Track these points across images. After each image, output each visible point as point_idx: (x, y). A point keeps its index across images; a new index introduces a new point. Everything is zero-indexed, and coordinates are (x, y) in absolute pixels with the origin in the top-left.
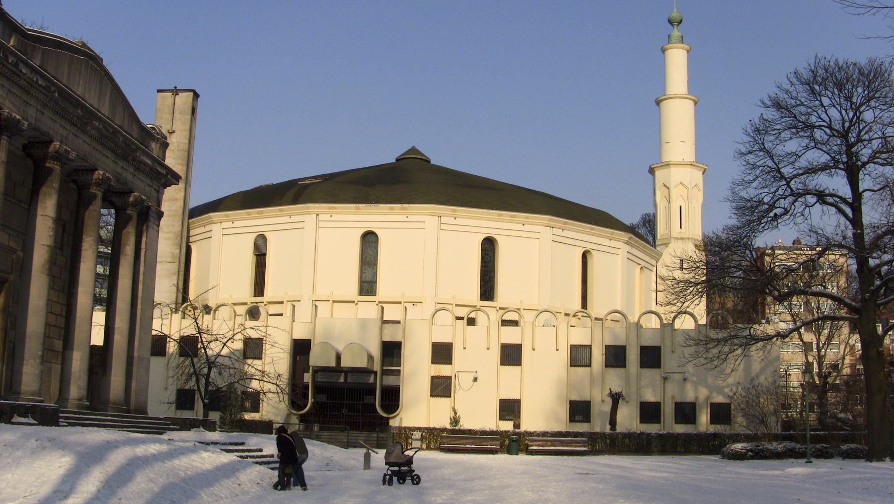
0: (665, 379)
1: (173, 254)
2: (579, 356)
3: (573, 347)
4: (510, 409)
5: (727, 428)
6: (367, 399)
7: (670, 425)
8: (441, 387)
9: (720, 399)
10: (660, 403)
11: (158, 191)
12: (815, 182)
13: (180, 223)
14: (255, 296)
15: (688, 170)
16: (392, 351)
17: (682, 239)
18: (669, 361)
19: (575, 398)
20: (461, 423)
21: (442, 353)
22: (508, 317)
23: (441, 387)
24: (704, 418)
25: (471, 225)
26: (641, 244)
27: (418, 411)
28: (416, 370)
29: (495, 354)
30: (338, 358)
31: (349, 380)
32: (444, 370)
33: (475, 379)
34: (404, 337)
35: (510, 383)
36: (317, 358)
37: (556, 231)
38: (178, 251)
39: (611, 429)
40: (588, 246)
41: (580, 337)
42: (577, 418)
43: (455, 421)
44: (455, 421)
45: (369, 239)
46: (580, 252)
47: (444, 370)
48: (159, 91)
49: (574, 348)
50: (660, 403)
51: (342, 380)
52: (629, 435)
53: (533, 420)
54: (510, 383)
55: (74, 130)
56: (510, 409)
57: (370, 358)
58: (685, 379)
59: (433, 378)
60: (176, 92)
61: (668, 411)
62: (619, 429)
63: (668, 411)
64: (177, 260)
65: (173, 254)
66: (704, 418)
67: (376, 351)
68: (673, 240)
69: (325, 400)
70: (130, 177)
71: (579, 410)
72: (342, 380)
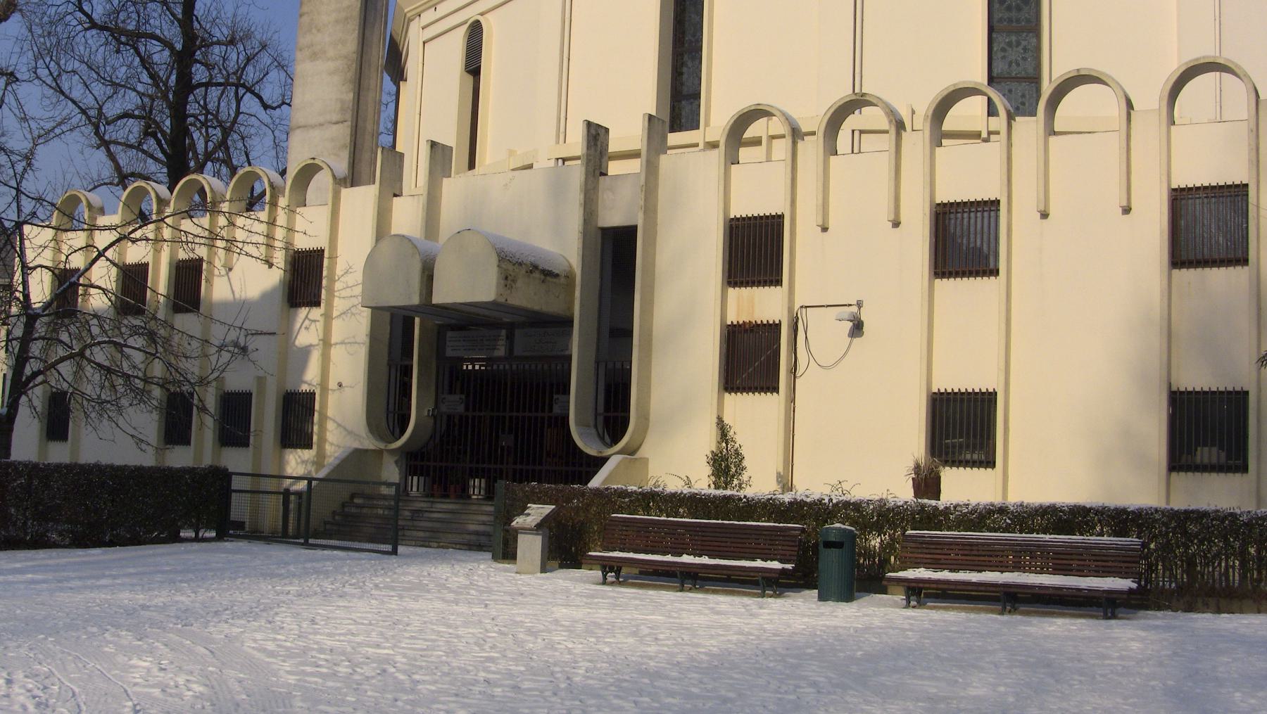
1: (342, 102)
3: (1180, 199)
4: (963, 425)
8: (752, 359)
10: (780, 217)
16: (617, 253)
19: (1195, 379)
28: (687, 302)
32: (760, 304)
33: (857, 328)
34: (650, 207)
35: (966, 336)
38: (351, 95)
42: (1205, 454)
47: (760, 304)
49: (1180, 199)
50: (780, 217)
54: (966, 336)
56: (963, 425)
64: (348, 116)
65: (342, 102)
69: (461, 409)
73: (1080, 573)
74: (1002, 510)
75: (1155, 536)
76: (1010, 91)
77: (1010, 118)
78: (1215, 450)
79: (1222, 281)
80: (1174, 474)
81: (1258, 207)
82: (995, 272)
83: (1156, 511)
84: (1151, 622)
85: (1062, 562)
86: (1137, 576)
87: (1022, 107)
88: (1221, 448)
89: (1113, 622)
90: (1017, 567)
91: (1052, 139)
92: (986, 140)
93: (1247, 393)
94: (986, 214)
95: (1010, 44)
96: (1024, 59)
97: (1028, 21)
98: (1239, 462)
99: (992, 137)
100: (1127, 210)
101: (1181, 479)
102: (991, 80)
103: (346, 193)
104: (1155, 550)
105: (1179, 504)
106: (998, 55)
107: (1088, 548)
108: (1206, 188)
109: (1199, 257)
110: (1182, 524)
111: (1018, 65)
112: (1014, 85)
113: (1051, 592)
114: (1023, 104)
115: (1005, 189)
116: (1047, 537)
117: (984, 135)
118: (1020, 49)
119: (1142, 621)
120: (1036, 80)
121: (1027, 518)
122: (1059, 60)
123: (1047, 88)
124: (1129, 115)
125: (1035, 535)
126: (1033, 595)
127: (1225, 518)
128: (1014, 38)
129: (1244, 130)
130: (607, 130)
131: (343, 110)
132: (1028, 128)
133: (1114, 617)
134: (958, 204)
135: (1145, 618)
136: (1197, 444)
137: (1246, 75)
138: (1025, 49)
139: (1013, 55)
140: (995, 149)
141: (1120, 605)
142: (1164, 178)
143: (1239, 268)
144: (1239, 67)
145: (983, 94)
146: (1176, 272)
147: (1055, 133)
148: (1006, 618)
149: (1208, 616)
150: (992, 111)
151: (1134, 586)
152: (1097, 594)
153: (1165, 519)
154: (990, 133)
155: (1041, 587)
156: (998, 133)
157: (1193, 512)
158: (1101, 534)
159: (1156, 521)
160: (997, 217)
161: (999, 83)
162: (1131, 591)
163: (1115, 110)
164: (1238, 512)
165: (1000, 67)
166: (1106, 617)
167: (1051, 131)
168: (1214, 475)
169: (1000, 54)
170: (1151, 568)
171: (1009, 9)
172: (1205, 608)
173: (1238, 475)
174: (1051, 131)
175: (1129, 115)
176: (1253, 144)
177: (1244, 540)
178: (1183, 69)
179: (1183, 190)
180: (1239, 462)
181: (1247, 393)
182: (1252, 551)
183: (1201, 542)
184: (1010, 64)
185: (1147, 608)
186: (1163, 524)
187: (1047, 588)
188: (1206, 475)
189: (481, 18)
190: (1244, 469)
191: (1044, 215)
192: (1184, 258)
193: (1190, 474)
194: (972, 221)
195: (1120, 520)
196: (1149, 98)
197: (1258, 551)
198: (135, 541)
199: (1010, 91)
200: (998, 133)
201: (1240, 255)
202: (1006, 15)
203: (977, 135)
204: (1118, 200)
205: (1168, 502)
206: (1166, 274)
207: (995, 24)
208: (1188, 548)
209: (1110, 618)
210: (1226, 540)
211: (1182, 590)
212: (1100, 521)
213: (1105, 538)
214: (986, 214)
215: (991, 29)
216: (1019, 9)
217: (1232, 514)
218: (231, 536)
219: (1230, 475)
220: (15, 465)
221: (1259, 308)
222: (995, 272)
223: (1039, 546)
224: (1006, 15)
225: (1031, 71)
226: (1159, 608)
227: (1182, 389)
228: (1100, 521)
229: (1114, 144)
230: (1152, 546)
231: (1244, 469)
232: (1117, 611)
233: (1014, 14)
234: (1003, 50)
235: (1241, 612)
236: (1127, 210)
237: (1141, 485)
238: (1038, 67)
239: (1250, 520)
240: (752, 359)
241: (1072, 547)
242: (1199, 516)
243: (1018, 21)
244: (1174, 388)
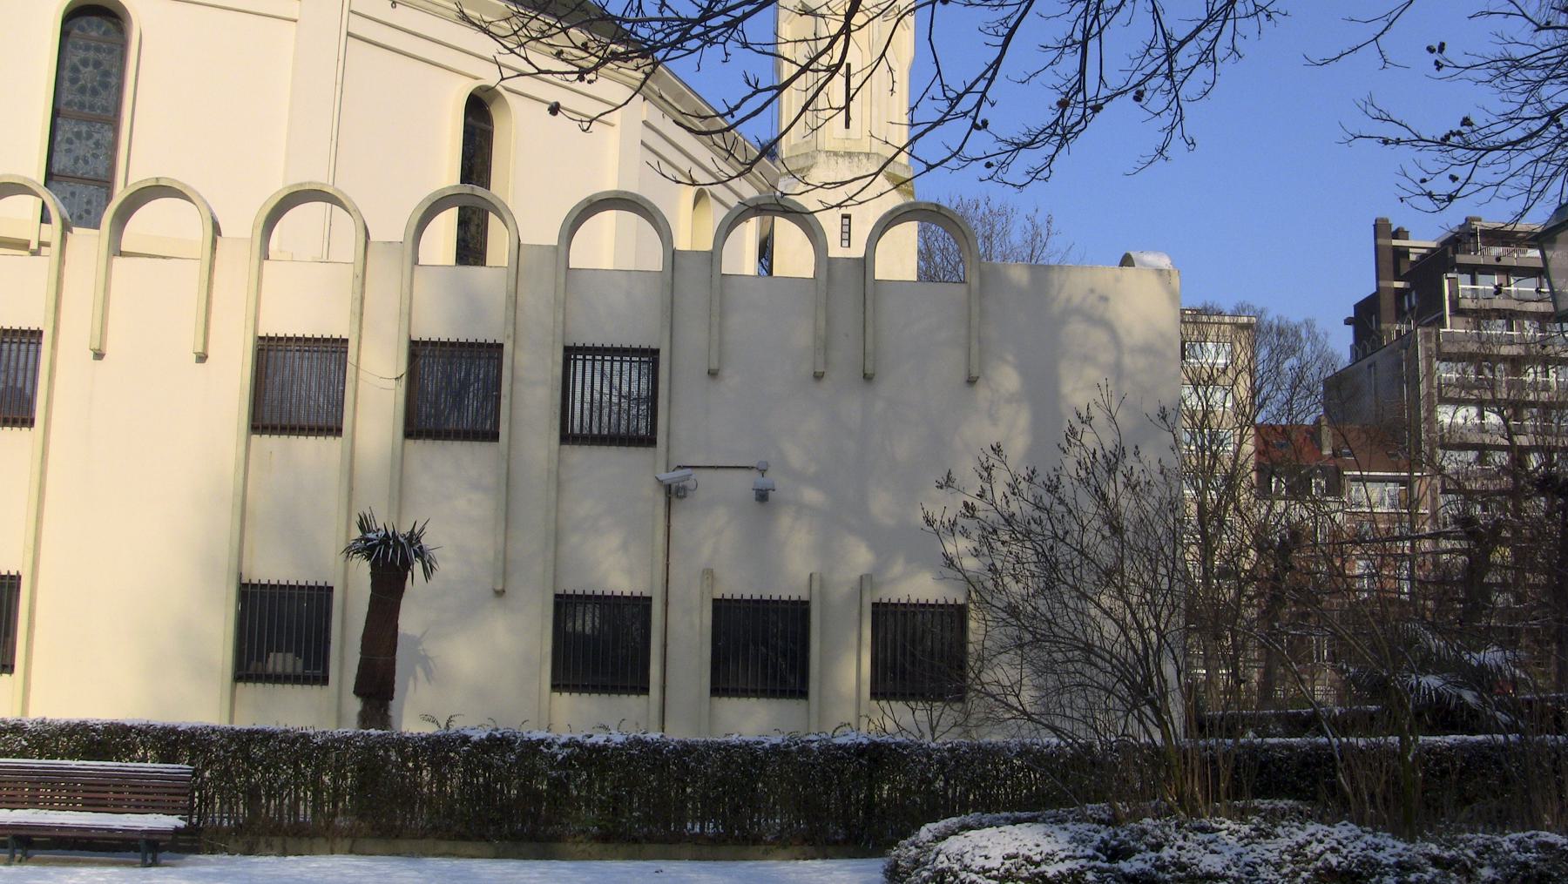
0: (673, 493)
2: (292, 388)
3: (268, 351)
5: (948, 714)
7: (684, 707)
9: (921, 586)
12: (953, 844)
13: (358, 435)
17: (850, 155)
18: (696, 423)
19: (273, 568)
24: (846, 667)
39: (365, 719)
40: (490, 77)
42: (279, 661)
46: (459, 93)
49: (268, 351)
52: (496, 753)
58: (762, 496)
61: (684, 642)
62: (413, 717)
63: (684, 642)
66: (846, 667)
68: (822, 158)
69: (1424, 680)
71: (275, 628)
73: (117, 809)
74: (17, 729)
75: (211, 763)
76: (73, 194)
77: (66, 228)
78: (290, 656)
79: (311, 453)
80: (240, 685)
81: (357, 368)
82: (28, 422)
83: (214, 730)
84: (202, 869)
85: (95, 795)
86: (187, 811)
87: (84, 216)
88: (298, 654)
89: (153, 870)
90: (34, 803)
91: (118, 262)
92: (35, 253)
93: (331, 588)
94: (14, 346)
95: (78, 135)
96: (95, 156)
97: (105, 109)
98: (319, 672)
99: (44, 250)
100: (202, 358)
101: (249, 691)
102: (50, 176)
104: (210, 779)
105: (243, 723)
106: (62, 147)
107: (126, 776)
108: (298, 339)
109: (294, 422)
110: (243, 747)
111: (86, 162)
112: (79, 188)
113: (74, 833)
114: (88, 212)
115: (51, 316)
116: (74, 763)
117: (34, 246)
118: (91, 143)
119: (190, 868)
120: (105, 183)
121: (48, 739)
122: (137, 163)
123: (120, 193)
124: (214, 242)
125: (58, 761)
126: (52, 837)
127: (295, 740)
128: (84, 128)
129: (348, 274)
132: (88, 243)
133: (155, 863)
134: (15, 332)
135: (194, 864)
136: (270, 650)
137: (357, 210)
138: (97, 144)
139: (81, 149)
140: (45, 264)
141: (163, 850)
142: (251, 323)
143: (330, 439)
144: (349, 200)
145: (37, 195)
146: (255, 438)
147: (122, 254)
148: (13, 869)
149: (272, 859)
150: (45, 218)
151: (182, 824)
152: (135, 836)
153: (225, 741)
154: (41, 244)
155: (62, 828)
156: (47, 245)
157: (257, 732)
158: (144, 760)
159: (211, 742)
160: (38, 352)
161: (59, 182)
162: (177, 830)
163: (199, 233)
164: (311, 732)
165: (62, 162)
166: (145, 865)
167: (116, 251)
168: (288, 687)
169: (65, 146)
170: (206, 801)
171: (82, 90)
172: (269, 850)
173: (316, 688)
174: (116, 251)
175: (214, 242)
176: (358, 291)
177: (317, 766)
178: (286, 193)
179: (271, 339)
180: (319, 672)
181: (331, 588)
182: (326, 779)
183: (267, 770)
184: (76, 160)
185: (197, 851)
186: (222, 746)
187: (70, 828)
188: (278, 686)
190: (324, 681)
191: (99, 355)
192: (267, 422)
193: (259, 685)
194: (14, 354)
195: (168, 741)
196: (241, 225)
197: (334, 780)
199: (73, 194)
200: (47, 245)
201: (332, 423)
202: (78, 98)
203: (24, 245)
204: (192, 345)
205: (231, 719)
206: (243, 438)
207: (63, 108)
208: (249, 776)
209: (150, 866)
210: (296, 765)
211: (239, 830)
212: (143, 743)
213: (149, 764)
214: (23, 347)
215: (56, 113)
216: (95, 92)
217: (303, 735)
218: (696, 839)
219: (307, 688)
220: (402, 743)
221: (351, 489)
222: (28, 422)
223: (63, 775)
224: (78, 98)
225: (102, 171)
226: (213, 851)
227: (255, 581)
228: (143, 743)
229: (194, 273)
230: (207, 774)
231: (324, 681)
232: (160, 856)
233: (87, 98)
234: (70, 141)
235: (311, 853)
236: (202, 358)
237: (200, 698)
238: (112, 169)
239: (325, 742)
241: (105, 776)
242: (266, 736)
243: (92, 107)
244: (245, 580)
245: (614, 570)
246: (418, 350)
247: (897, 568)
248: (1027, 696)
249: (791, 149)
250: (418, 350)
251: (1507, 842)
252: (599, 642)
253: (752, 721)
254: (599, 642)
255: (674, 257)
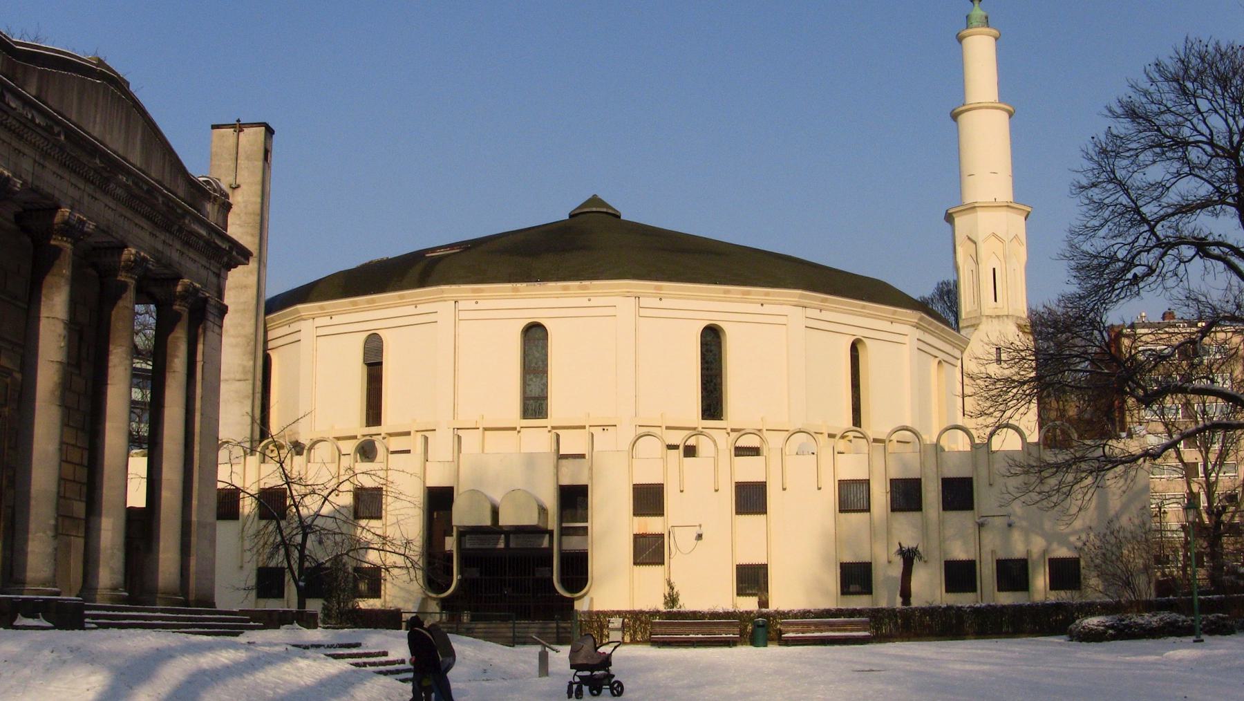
0: (981, 526)
1: (244, 367)
2: (852, 497)
3: (844, 485)
4: (752, 578)
5: (1076, 594)
6: (540, 573)
9: (1063, 552)
11: (218, 276)
14: (368, 425)
15: (1003, 214)
16: (574, 499)
17: (998, 317)
18: (985, 499)
19: (848, 559)
20: (681, 602)
21: (649, 499)
22: (746, 442)
23: (649, 551)
24: (1040, 581)
25: (690, 305)
26: (937, 328)
27: (616, 586)
28: (611, 527)
29: (728, 498)
30: (495, 512)
31: (512, 545)
32: (652, 525)
33: (700, 537)
34: (591, 478)
35: (750, 540)
36: (463, 514)
37: (810, 313)
39: (904, 603)
40: (860, 333)
41: (852, 469)
42: (852, 588)
43: (672, 599)
44: (672, 599)
45: (534, 335)
46: (848, 341)
47: (652, 525)
48: (214, 127)
49: (844, 485)
51: (501, 545)
52: (931, 611)
53: (786, 595)
54: (750, 540)
55: (90, 189)
56: (752, 578)
57: (543, 510)
58: (1010, 525)
59: (637, 537)
60: (239, 127)
61: (987, 574)
62: (915, 602)
63: (987, 574)
64: (250, 376)
65: (244, 367)
66: (1040, 581)
67: (550, 500)
68: (984, 319)
69: (477, 575)
70: (175, 256)
71: (855, 577)
72: (501, 545)
103: (249, 458)
130: (595, 200)
131: (245, 372)
189: (518, 421)
191: (784, 489)
198: (1011, 131)
240: (649, 551)
245: (959, 553)
246: (893, 482)
247: (1055, 546)
248: (1101, 588)
249: (967, 313)
250: (893, 482)
251: (1210, 617)
252: (960, 575)
253: (1006, 599)
254: (960, 575)
255: (974, 445)
